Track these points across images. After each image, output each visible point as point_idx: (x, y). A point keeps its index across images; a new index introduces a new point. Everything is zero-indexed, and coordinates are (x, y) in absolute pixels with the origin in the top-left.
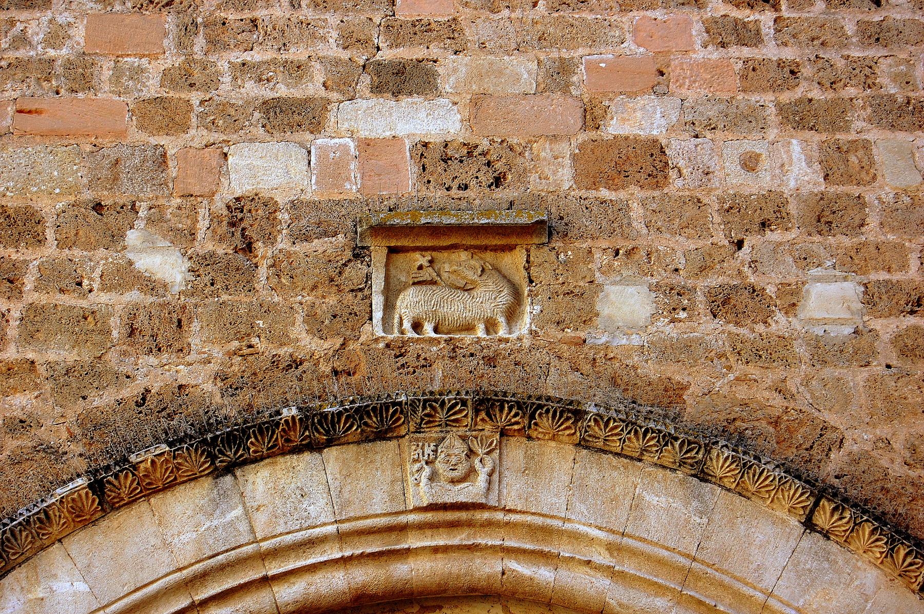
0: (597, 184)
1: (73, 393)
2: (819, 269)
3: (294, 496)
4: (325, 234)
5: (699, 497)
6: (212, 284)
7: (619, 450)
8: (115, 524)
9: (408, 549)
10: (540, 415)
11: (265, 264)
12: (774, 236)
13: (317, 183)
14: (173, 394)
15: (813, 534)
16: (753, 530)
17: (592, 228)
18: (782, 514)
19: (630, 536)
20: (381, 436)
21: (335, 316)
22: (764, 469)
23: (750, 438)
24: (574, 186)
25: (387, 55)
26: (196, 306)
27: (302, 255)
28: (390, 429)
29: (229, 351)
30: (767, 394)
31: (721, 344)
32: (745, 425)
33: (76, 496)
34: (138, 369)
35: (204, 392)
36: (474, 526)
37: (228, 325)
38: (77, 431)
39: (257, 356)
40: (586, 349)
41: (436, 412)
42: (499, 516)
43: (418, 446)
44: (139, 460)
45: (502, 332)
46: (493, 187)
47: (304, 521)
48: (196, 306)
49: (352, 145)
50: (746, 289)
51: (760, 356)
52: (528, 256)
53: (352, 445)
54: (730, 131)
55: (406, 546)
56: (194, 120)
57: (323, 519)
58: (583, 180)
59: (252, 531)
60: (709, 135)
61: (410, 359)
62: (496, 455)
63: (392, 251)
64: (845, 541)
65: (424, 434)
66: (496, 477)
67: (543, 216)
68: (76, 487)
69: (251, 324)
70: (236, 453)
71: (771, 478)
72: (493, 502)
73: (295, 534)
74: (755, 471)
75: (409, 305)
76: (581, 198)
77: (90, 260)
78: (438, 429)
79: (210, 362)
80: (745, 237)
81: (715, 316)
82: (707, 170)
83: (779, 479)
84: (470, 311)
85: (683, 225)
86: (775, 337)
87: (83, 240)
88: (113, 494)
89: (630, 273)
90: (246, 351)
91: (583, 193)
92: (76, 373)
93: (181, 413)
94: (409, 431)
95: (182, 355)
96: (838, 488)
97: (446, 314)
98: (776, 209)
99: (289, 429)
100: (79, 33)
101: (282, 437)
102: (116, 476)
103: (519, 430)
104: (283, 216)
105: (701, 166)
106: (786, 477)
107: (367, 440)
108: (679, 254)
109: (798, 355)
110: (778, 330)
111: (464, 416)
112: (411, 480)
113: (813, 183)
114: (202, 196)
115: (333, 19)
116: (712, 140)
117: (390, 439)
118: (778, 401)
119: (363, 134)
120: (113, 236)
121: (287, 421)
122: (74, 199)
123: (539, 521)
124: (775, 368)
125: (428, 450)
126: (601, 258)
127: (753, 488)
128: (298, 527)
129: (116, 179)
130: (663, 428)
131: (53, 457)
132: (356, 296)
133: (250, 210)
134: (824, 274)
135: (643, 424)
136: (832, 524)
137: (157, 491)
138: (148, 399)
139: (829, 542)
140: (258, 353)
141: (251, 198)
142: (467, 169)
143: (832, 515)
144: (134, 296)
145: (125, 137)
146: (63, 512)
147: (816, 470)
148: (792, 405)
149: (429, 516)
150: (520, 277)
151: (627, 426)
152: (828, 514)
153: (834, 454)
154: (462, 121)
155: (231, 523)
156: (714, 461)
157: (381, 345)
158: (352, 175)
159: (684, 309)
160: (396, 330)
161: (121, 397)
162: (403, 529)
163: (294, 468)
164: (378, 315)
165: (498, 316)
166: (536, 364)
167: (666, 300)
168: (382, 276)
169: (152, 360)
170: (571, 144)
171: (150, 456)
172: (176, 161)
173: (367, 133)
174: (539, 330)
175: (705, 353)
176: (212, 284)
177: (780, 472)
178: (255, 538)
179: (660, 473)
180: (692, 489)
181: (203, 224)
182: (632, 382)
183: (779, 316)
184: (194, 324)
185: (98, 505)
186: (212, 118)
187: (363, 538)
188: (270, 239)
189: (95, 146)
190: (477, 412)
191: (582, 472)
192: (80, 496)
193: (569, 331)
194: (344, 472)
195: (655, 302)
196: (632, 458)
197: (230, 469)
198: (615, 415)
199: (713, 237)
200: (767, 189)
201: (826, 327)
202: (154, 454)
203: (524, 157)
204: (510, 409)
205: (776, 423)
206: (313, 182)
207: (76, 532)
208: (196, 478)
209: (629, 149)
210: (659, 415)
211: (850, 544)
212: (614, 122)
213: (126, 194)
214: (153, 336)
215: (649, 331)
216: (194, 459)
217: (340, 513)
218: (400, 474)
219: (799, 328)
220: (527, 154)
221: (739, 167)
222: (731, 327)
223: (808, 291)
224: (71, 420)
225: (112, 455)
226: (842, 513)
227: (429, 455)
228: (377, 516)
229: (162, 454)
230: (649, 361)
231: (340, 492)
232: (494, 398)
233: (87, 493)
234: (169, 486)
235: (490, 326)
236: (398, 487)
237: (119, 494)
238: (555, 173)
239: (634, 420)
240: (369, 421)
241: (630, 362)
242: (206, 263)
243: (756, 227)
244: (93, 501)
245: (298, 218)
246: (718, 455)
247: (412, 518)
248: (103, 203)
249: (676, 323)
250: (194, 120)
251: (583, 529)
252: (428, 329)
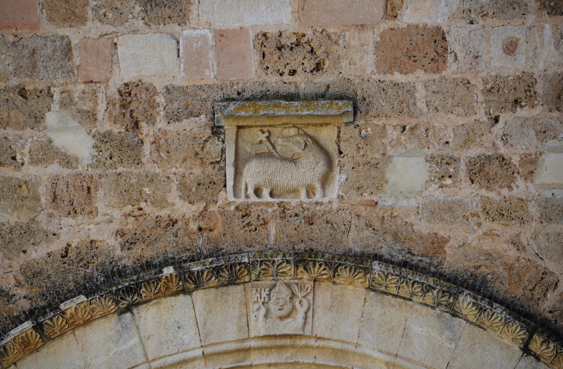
0: (392, 68)
1: (16, 248)
2: (555, 140)
3: (173, 328)
4: (192, 114)
5: (450, 328)
6: (111, 158)
7: (396, 293)
8: (52, 350)
9: (251, 365)
10: (341, 269)
11: (148, 141)
12: (523, 113)
13: (185, 70)
14: (87, 248)
15: (528, 357)
16: (486, 353)
17: (387, 108)
18: (507, 341)
19: (401, 357)
20: (232, 282)
21: (199, 184)
22: (495, 312)
23: (490, 281)
24: (375, 71)
26: (100, 176)
27: (175, 134)
28: (238, 278)
29: (125, 213)
30: (505, 246)
31: (475, 206)
32: (488, 271)
33: (24, 335)
34: (61, 228)
35: (109, 245)
36: (296, 348)
37: (124, 192)
38: (21, 278)
39: (145, 216)
40: (377, 210)
41: (269, 267)
42: (312, 342)
43: (257, 290)
44: (66, 308)
45: (318, 197)
46: (314, 72)
47: (180, 347)
48: (100, 176)
49: (210, 35)
50: (497, 158)
51: (503, 215)
52: (339, 132)
53: (212, 289)
54: (497, 17)
55: (249, 363)
56: (90, 13)
57: (192, 345)
58: (382, 65)
59: (146, 355)
60: (481, 22)
61: (252, 219)
62: (310, 297)
63: (239, 127)
64: (551, 363)
65: (261, 282)
66: (310, 314)
67: (348, 107)
68: (24, 329)
69: (140, 191)
70: (132, 298)
71: (500, 318)
72: (308, 333)
73: (174, 356)
74: (489, 313)
75: (252, 175)
76: (380, 81)
77: (21, 138)
78: (271, 278)
79: (112, 222)
80: (500, 114)
81: (472, 181)
82: (476, 55)
83: (505, 319)
84: (295, 179)
85: (455, 104)
86: (515, 199)
87: (14, 120)
88: (50, 331)
89: (413, 146)
90: (137, 213)
91: (381, 77)
92: (17, 232)
93: (94, 263)
94: (251, 279)
95: (92, 216)
96: (551, 321)
97: (278, 182)
98: (527, 88)
99: (168, 281)
101: (164, 286)
102: (51, 319)
103: (327, 279)
104: (160, 99)
105: (472, 51)
106: (509, 319)
107: (223, 285)
108: (450, 130)
109: (530, 214)
110: (518, 194)
111: (289, 270)
112: (252, 316)
113: (558, 64)
114: (100, 82)
116: (483, 27)
117: (238, 284)
118: (513, 253)
119: (219, 25)
120: (36, 118)
121: (166, 277)
122: (4, 85)
123: (339, 346)
124: (513, 225)
125: (264, 295)
126: (393, 134)
127: (488, 324)
128: (176, 351)
129: (34, 67)
130: (425, 282)
131: (5, 299)
132: (215, 167)
133: (136, 94)
134: (558, 144)
135: (412, 278)
136: (542, 351)
137: (79, 326)
138: (70, 251)
139: (540, 363)
140: (146, 215)
141: (136, 84)
142: (296, 56)
143: (542, 345)
144: (55, 168)
145: (39, 29)
146: (16, 346)
147: (536, 306)
148: (522, 255)
149: (265, 343)
150: (332, 148)
151: (400, 278)
152: (539, 345)
153: (550, 294)
154: (292, 13)
155: (131, 349)
156: (461, 304)
157: (232, 208)
158: (210, 63)
159: (450, 177)
160: (243, 195)
161: (50, 250)
162: (248, 350)
163: (172, 307)
164: (230, 183)
165: (316, 183)
166: (341, 222)
167: (437, 169)
168: (233, 150)
169: (71, 221)
170: (374, 33)
171: (74, 305)
172: (78, 51)
173: (221, 25)
174: (344, 195)
175: (463, 213)
176: (111, 158)
177: (506, 315)
178: (147, 359)
179: (425, 309)
180: (445, 322)
181: (102, 107)
182: (409, 237)
183: (520, 182)
184: (100, 192)
185: (40, 338)
186: (104, 11)
187: (221, 357)
188: (151, 120)
189: (16, 36)
190: (297, 267)
191: (370, 309)
192: (27, 335)
193: (366, 195)
194: (207, 310)
195: (429, 171)
196: (405, 298)
197: (128, 309)
198: (392, 272)
199: (476, 114)
200: (521, 70)
201: (554, 191)
202: (77, 303)
203: (338, 45)
204: (320, 265)
205: (510, 268)
206: (182, 69)
207: (25, 357)
208: (106, 315)
209: (418, 36)
210: (427, 263)
211: (554, 365)
212: (408, 11)
213: (43, 81)
214: (71, 201)
215: (423, 195)
216: (104, 304)
217: (205, 340)
218: (245, 311)
219: (533, 191)
220: (341, 42)
221: (501, 51)
222: (484, 192)
223: (543, 161)
224: (16, 269)
225: (47, 297)
226: (548, 345)
227: (264, 298)
228: (229, 342)
229: (83, 302)
230: (422, 220)
231: (204, 324)
232: (309, 259)
233: (31, 333)
234: (87, 322)
235: (310, 192)
236: (244, 321)
237: (54, 330)
238: (361, 58)
239: (405, 276)
240: (223, 275)
241: (408, 220)
242: (105, 140)
243: (509, 105)
244: (36, 336)
245: (171, 101)
246: (463, 300)
247: (253, 343)
248: (26, 88)
249: (443, 188)
250: (90, 13)
251: (369, 352)
252: (266, 193)
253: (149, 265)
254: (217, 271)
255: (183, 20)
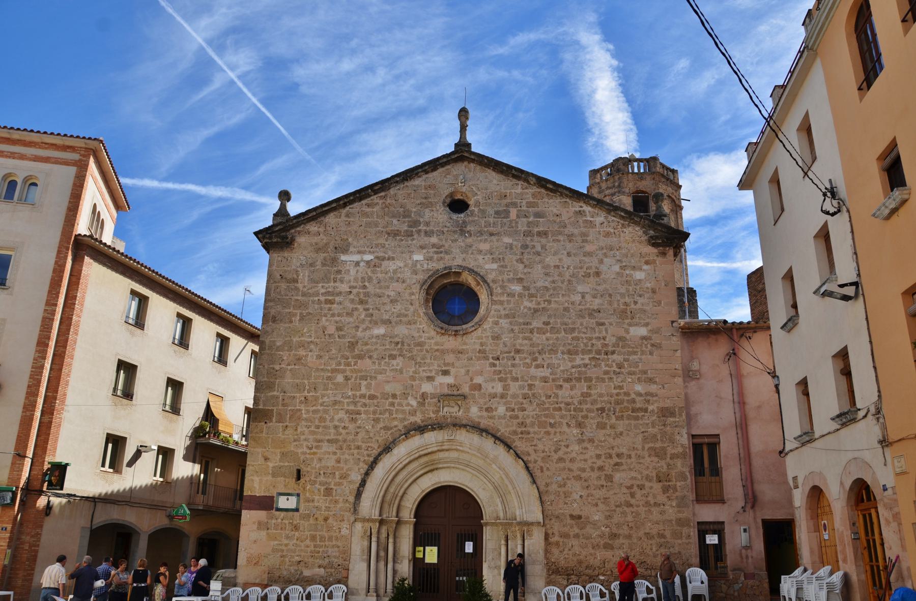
20: (441, 429)
25: (444, 368)
100: (401, 364)
115: (436, 362)
126: (471, 402)
144: (410, 407)
188: (427, 399)
235: (456, 413)
253: (426, 426)
254: (438, 427)
255: (434, 381)
